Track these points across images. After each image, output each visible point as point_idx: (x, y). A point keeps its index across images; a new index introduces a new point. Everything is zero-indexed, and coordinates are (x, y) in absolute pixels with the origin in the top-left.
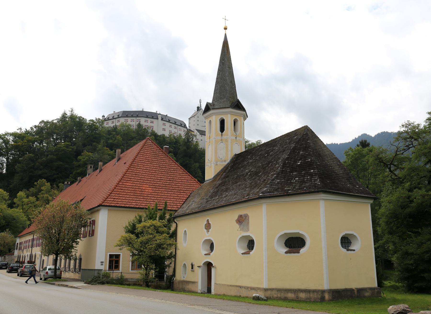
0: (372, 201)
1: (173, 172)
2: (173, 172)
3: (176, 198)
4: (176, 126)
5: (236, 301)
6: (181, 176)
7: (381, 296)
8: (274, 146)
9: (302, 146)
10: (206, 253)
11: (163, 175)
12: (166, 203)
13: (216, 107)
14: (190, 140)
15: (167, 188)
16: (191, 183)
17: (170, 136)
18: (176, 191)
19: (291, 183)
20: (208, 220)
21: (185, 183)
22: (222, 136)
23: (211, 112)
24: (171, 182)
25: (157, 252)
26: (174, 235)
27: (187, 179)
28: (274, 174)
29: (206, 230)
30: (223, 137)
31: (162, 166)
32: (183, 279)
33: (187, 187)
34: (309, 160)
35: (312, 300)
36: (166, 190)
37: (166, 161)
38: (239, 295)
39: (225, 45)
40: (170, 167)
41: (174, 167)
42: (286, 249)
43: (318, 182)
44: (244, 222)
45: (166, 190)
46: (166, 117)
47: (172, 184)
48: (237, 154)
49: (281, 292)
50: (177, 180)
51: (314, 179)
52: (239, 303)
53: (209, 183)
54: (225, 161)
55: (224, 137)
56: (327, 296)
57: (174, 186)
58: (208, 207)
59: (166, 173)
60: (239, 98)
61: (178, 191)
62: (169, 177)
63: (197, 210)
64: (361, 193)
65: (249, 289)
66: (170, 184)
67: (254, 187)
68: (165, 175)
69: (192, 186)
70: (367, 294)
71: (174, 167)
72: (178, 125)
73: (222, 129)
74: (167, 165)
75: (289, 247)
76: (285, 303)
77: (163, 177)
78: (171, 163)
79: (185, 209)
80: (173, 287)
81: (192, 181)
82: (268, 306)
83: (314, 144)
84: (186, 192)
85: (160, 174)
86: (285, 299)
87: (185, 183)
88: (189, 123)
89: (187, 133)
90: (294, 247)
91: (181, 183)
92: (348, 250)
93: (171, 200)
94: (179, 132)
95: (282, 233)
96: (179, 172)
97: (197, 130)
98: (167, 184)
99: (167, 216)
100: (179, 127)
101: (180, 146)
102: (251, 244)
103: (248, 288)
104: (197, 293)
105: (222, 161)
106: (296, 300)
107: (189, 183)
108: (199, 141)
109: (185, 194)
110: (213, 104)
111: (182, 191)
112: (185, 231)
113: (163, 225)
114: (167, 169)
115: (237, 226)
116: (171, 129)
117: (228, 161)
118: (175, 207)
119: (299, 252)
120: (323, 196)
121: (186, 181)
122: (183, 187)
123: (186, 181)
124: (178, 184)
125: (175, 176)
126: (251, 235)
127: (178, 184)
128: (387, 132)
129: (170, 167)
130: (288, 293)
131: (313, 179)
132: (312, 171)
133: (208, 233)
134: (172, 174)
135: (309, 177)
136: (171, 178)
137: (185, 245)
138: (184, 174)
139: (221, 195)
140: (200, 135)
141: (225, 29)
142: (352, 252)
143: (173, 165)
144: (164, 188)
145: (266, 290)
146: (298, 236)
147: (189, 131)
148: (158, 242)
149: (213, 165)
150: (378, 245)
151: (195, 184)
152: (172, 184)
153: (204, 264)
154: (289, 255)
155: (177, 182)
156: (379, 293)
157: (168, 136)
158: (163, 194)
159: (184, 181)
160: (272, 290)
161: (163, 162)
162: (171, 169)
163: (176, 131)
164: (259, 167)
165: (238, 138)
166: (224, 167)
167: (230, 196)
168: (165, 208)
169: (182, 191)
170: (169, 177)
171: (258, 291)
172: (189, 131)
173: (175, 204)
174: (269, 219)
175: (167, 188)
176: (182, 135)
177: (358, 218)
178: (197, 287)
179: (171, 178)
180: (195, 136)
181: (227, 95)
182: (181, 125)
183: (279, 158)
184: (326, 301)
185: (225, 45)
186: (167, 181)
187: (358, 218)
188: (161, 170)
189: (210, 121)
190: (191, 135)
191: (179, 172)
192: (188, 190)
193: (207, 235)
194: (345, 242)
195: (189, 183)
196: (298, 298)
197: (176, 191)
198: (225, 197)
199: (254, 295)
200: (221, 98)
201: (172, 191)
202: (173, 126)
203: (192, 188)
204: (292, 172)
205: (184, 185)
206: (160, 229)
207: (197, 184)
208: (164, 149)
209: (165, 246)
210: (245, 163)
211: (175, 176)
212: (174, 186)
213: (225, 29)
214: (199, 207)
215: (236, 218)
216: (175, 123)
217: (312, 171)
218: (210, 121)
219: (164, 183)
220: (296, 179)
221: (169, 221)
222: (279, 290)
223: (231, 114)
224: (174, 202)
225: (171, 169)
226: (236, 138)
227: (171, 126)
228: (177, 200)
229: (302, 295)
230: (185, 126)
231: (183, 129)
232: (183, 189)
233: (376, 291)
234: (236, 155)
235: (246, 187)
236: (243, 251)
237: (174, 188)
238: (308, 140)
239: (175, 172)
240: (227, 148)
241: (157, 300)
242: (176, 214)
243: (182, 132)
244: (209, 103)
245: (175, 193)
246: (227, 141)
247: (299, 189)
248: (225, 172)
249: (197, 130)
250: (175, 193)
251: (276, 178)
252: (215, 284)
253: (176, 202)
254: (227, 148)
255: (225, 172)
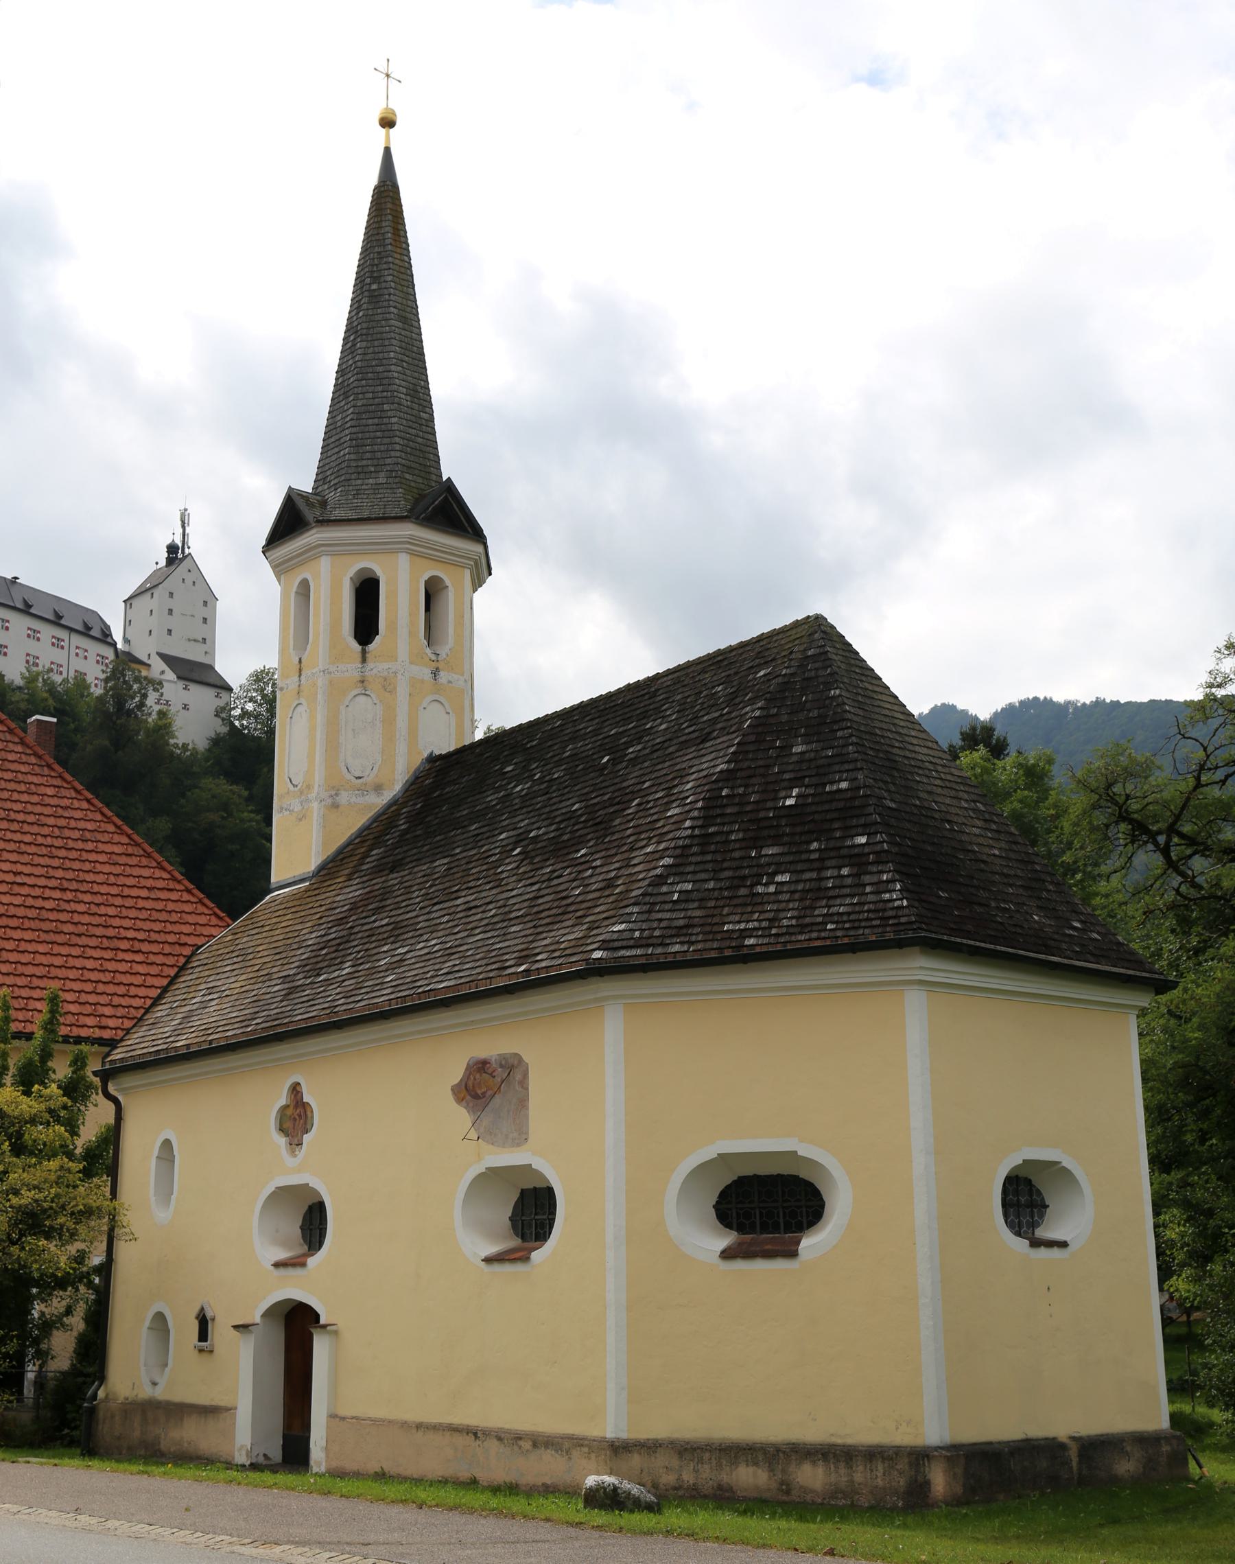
0: (1144, 1000)
1: (80, 845)
2: (80, 845)
3: (94, 976)
4: (63, 634)
5: (498, 1513)
6: (117, 870)
7: (1188, 1479)
8: (645, 716)
9: (802, 716)
10: (282, 1255)
11: (26, 859)
12: (54, 1001)
13: (337, 514)
14: (132, 704)
15: (46, 926)
16: (171, 906)
17: (31, 680)
18: (93, 942)
19: (756, 901)
20: (295, 1089)
21: (141, 904)
22: (364, 660)
23: (313, 536)
24: (69, 895)
25: (14, 1250)
26: (104, 1158)
27: (149, 883)
28: (661, 855)
29: (282, 1141)
30: (370, 665)
31: (21, 817)
32: (146, 1392)
33: (147, 925)
34: (844, 785)
35: (864, 1501)
36: (44, 937)
37: (42, 790)
38: (464, 1475)
39: (386, 203)
40: (62, 822)
41: (82, 825)
42: (726, 1239)
43: (895, 896)
44: (497, 1100)
45: (44, 937)
46: (14, 590)
47: (73, 906)
48: (441, 757)
49: (701, 1461)
50: (96, 888)
51: (875, 879)
52: (516, 1528)
53: (293, 897)
54: (378, 788)
55: (377, 667)
56: (939, 1481)
57: (86, 919)
58: (300, 1016)
59: (44, 851)
60: (448, 470)
61: (106, 943)
62: (60, 874)
63: (233, 1033)
64: (1098, 958)
65: (526, 1445)
66: (65, 906)
67: (556, 921)
68: (37, 860)
69: (175, 917)
70: (1125, 1467)
71: (82, 825)
72: (71, 630)
73: (366, 625)
74: (48, 811)
75: (741, 1229)
76: (727, 1521)
77: (27, 870)
78: (65, 802)
79: (166, 1029)
80: (90, 1433)
81: (174, 896)
82: (689, 1543)
83: (861, 705)
84: (145, 947)
85: (14, 857)
86: (723, 1498)
87: (141, 904)
88: (128, 623)
89: (114, 671)
90: (765, 1228)
91: (118, 901)
92: (1036, 1243)
93: (88, 975)
94: (78, 664)
95: (708, 1153)
96: (108, 848)
97: (165, 658)
98: (49, 904)
99: (61, 1069)
100: (77, 640)
101: (76, 730)
102: (533, 1212)
103: (518, 1437)
104: (229, 1465)
105: (362, 790)
106: (782, 1504)
107: (160, 906)
108: (173, 709)
109: (139, 958)
110: (317, 499)
111: (124, 945)
112: (167, 1144)
113: (51, 1111)
114: (46, 831)
115: (461, 1117)
116: (33, 647)
117: (395, 788)
118: (90, 1021)
119: (792, 1254)
120: (920, 965)
121: (144, 893)
122: (127, 923)
123: (144, 893)
124: (103, 910)
125: (87, 866)
126: (539, 1164)
127: (103, 910)
128: (1048, 702)
129: (62, 822)
130: (734, 1463)
131: (867, 879)
132: (863, 840)
133: (293, 1153)
134: (74, 854)
135: (845, 871)
136: (70, 875)
137: (162, 1215)
138: (134, 861)
139: (369, 956)
140: (181, 684)
141: (388, 123)
142: (1055, 1253)
143: (78, 814)
144: (33, 925)
145: (618, 1449)
146: (785, 1171)
147: (126, 660)
148: (27, 1197)
149: (315, 805)
150: (735, 1226)
151: (188, 908)
152: (73, 906)
153: (268, 1314)
154: (740, 1265)
155: (98, 899)
156: (1178, 1459)
157: (19, 682)
158: (25, 958)
159: (135, 892)
160: (650, 1447)
161: (25, 797)
162: (67, 833)
163: (59, 656)
164: (571, 816)
165: (444, 676)
166: (376, 819)
167: (416, 962)
168: (50, 1026)
169: (124, 945)
170: (60, 874)
171: (576, 1453)
172: (125, 663)
173: (88, 1009)
174: (633, 1086)
175: (46, 926)
176: (90, 679)
177: (1078, 1079)
178: (229, 1433)
179: (70, 875)
180: (158, 685)
181: (381, 467)
182: (86, 631)
183: (682, 775)
184: (934, 1505)
185: (386, 203)
186: (48, 893)
187: (1078, 1079)
188: (18, 837)
189: (305, 585)
190: (137, 679)
191: (108, 848)
192: (154, 936)
193: (290, 1161)
194: (1018, 1204)
195: (160, 906)
196: (788, 1492)
197: (93, 942)
198: (390, 968)
199: (591, 1481)
200: (362, 472)
201: (75, 940)
202: (47, 632)
203: (176, 928)
204: (756, 842)
205: (133, 913)
206: (38, 1134)
207: (201, 909)
208: (32, 730)
209: (61, 1220)
210: (492, 798)
211: (87, 866)
212: (86, 919)
213: (388, 123)
214: (245, 1021)
215: (457, 1074)
216: (56, 620)
217: (863, 840)
218: (305, 585)
219: (30, 902)
220: (779, 878)
221: (75, 1089)
222: (687, 1450)
223: (412, 553)
224: (84, 998)
225: (67, 833)
226: (435, 673)
227: (34, 635)
228: (101, 988)
229: (811, 1477)
230: (105, 637)
231: (95, 649)
232: (131, 934)
233: (1166, 1448)
234: (432, 759)
235: (507, 919)
236: (492, 1249)
237: (82, 929)
238: (828, 686)
239: (90, 846)
240: (389, 721)
241: (54, 1517)
242: (118, 1054)
243: (91, 667)
244: (301, 494)
245: (90, 952)
246: (388, 686)
247: (802, 928)
248: (378, 841)
249: (165, 658)
250: (90, 952)
251: (675, 871)
252: (332, 1416)
253: (92, 998)
254: (389, 721)
255: (378, 841)
